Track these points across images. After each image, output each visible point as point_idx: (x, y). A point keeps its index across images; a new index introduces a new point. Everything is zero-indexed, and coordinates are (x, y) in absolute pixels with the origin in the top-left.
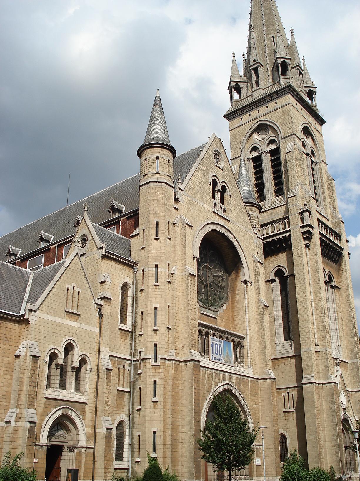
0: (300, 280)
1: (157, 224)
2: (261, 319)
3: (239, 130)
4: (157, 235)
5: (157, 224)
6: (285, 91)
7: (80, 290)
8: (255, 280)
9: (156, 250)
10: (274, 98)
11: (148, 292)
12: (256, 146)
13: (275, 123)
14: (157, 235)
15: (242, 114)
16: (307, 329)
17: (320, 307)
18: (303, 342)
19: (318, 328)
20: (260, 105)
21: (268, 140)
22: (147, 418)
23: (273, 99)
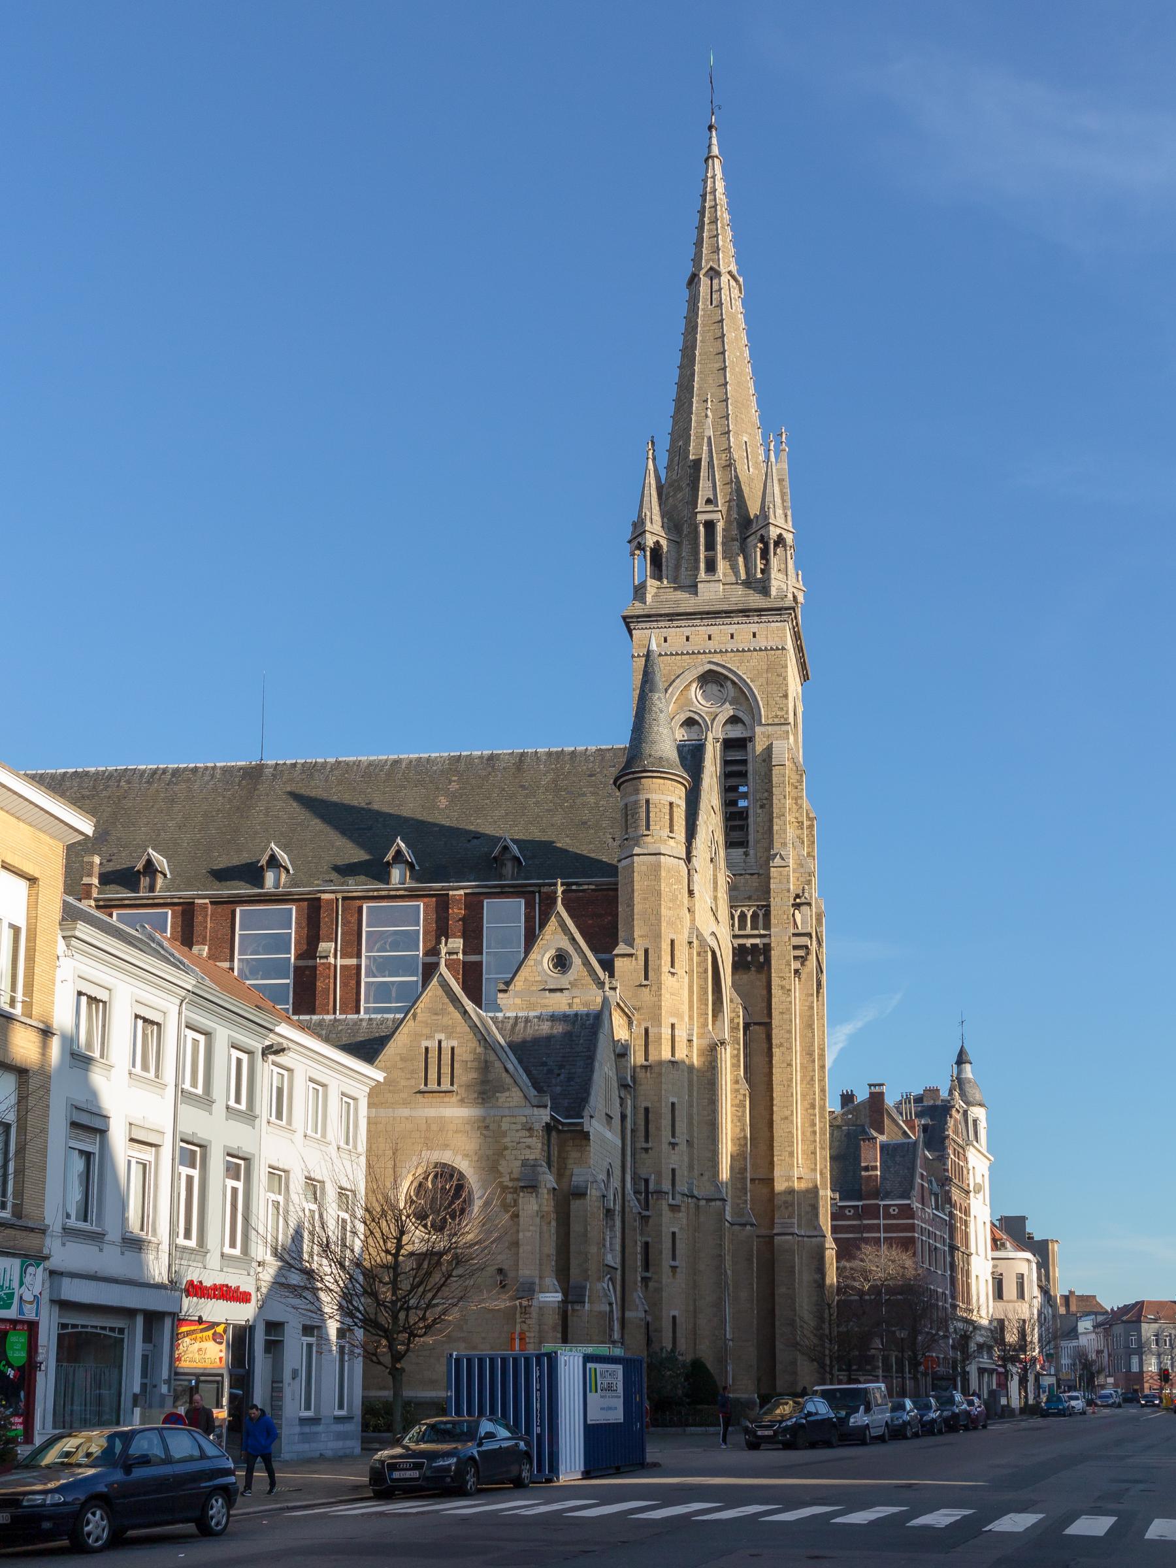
1: (672, 942)
2: (740, 1114)
5: (672, 942)
7: (455, 1043)
8: (732, 1039)
9: (672, 994)
11: (660, 1074)
12: (697, 717)
13: (748, 681)
14: (673, 966)
17: (811, 1097)
18: (779, 1157)
19: (803, 1133)
22: (664, 1294)
23: (748, 621)
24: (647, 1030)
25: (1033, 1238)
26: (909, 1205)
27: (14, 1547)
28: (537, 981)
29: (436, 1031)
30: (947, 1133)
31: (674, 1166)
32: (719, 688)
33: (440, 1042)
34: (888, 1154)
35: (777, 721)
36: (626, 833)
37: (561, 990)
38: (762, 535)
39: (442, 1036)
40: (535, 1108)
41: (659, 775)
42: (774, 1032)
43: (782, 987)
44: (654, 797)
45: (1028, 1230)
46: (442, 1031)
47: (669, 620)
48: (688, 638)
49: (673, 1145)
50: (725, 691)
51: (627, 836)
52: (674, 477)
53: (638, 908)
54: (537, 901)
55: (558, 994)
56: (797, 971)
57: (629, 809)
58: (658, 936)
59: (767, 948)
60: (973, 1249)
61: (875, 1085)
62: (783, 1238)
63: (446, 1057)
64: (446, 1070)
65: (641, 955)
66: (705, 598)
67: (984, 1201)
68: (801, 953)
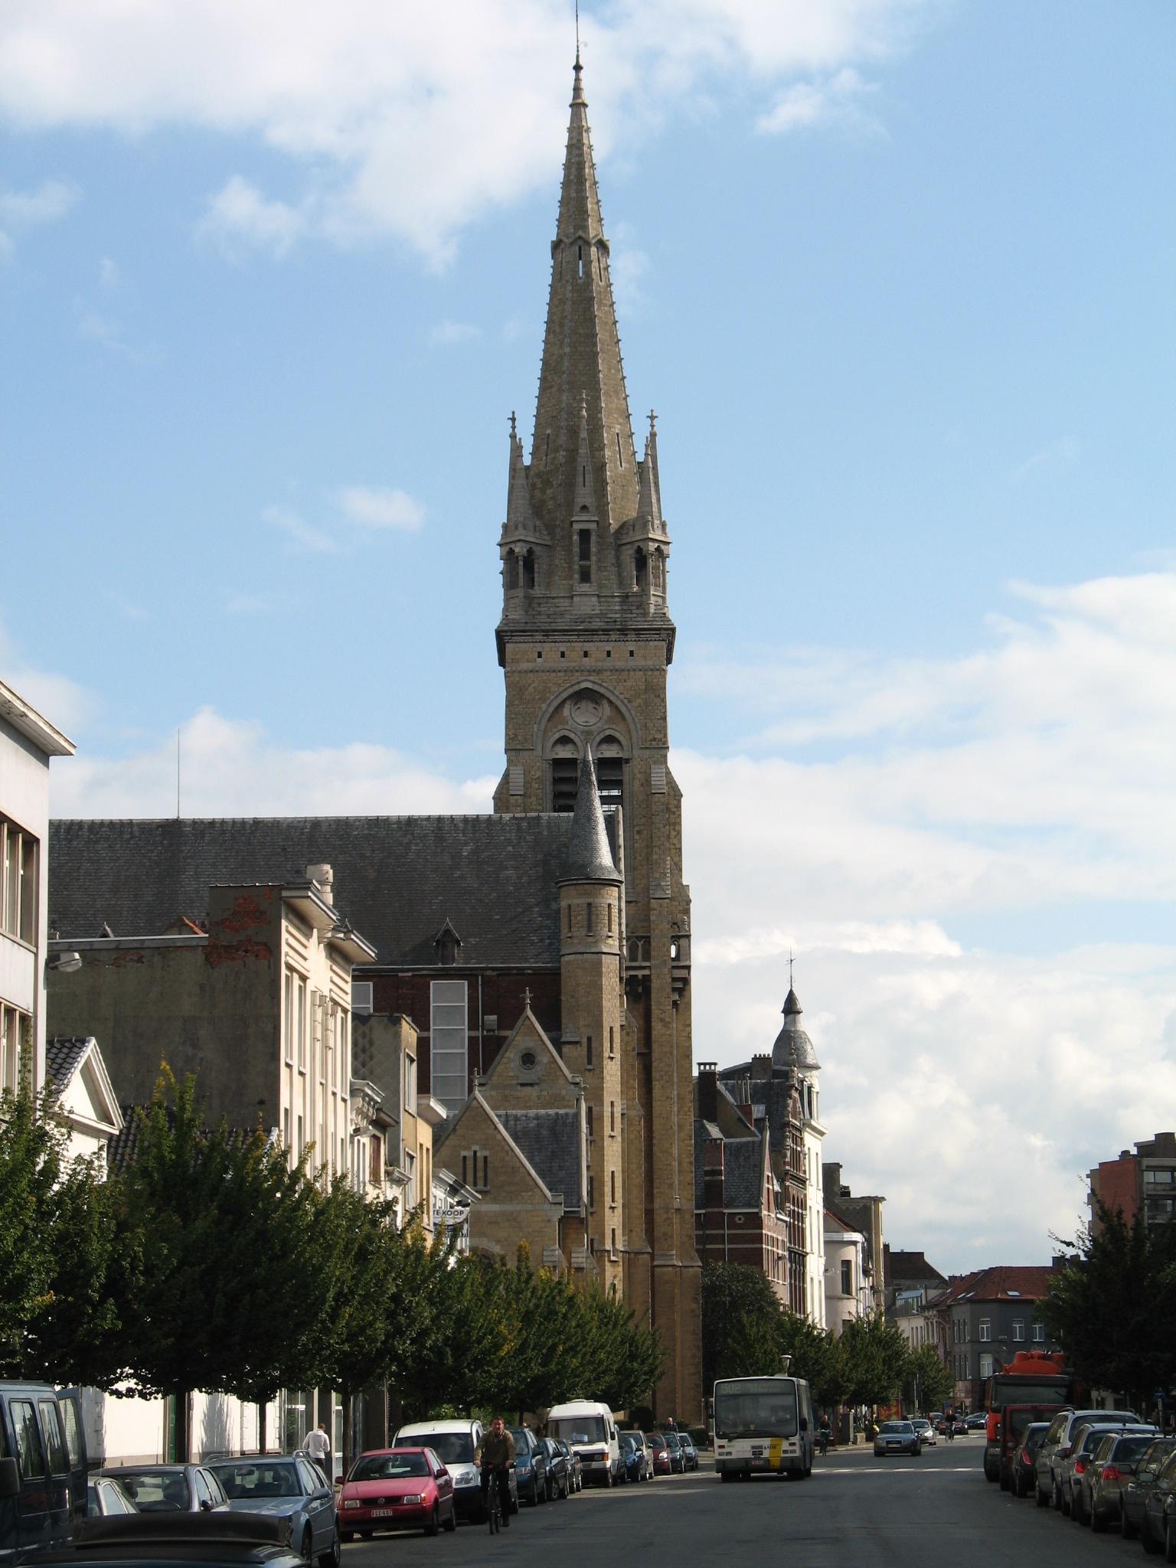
0: (662, 1073)
3: (533, 681)
4: (590, 1063)
6: (659, 634)
7: (487, 1153)
10: (629, 639)
15: (544, 642)
16: (669, 1168)
18: (658, 1190)
20: (592, 641)
21: (602, 736)
25: (848, 1194)
26: (757, 1213)
27: (213, 1536)
28: (511, 1077)
29: (473, 1144)
30: (787, 1119)
31: (613, 1227)
32: (594, 706)
33: (475, 1152)
34: (731, 1154)
36: (570, 931)
37: (531, 1085)
38: (639, 547)
39: (476, 1148)
40: (553, 1205)
41: (600, 882)
42: (654, 1064)
43: (662, 1020)
46: (477, 1144)
47: (544, 636)
49: (613, 1208)
50: (600, 709)
51: (570, 935)
52: (542, 468)
54: (480, 982)
55: (529, 1088)
56: (675, 1003)
57: (572, 910)
59: (647, 979)
60: (808, 1250)
61: (705, 1064)
62: (665, 1269)
63: (480, 1164)
64: (480, 1174)
65: (585, 1041)
66: (580, 612)
67: (818, 1186)
68: (679, 985)
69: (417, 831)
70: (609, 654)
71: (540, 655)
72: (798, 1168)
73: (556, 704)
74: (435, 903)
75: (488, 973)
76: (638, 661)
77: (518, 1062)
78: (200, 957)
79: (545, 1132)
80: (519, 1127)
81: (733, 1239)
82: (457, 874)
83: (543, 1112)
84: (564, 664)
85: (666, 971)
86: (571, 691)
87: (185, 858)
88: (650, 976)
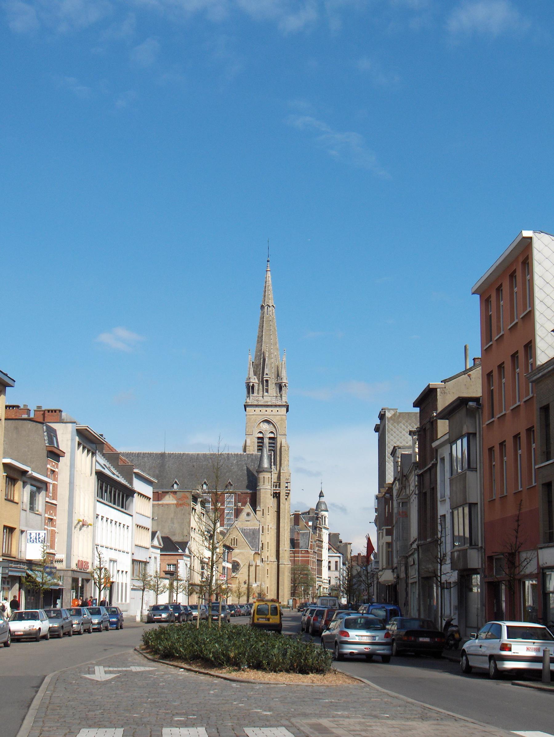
4: (263, 515)
7: (237, 538)
19: (287, 539)
21: (270, 431)
24: (263, 527)
35: (283, 434)
39: (234, 537)
43: (283, 503)
44: (265, 476)
45: (340, 538)
48: (260, 411)
49: (268, 551)
52: (257, 363)
53: (261, 500)
58: (265, 507)
59: (279, 493)
64: (235, 543)
65: (262, 510)
68: (287, 494)
69: (223, 457)
70: (272, 411)
71: (255, 411)
72: (321, 538)
73: (258, 423)
74: (194, 715)
75: (239, 493)
76: (279, 413)
77: (245, 515)
78: (175, 506)
79: (251, 533)
80: (245, 532)
81: (302, 557)
82: (232, 467)
83: (251, 528)
84: (261, 413)
85: (284, 491)
86: (262, 420)
87: (166, 462)
88: (280, 492)
